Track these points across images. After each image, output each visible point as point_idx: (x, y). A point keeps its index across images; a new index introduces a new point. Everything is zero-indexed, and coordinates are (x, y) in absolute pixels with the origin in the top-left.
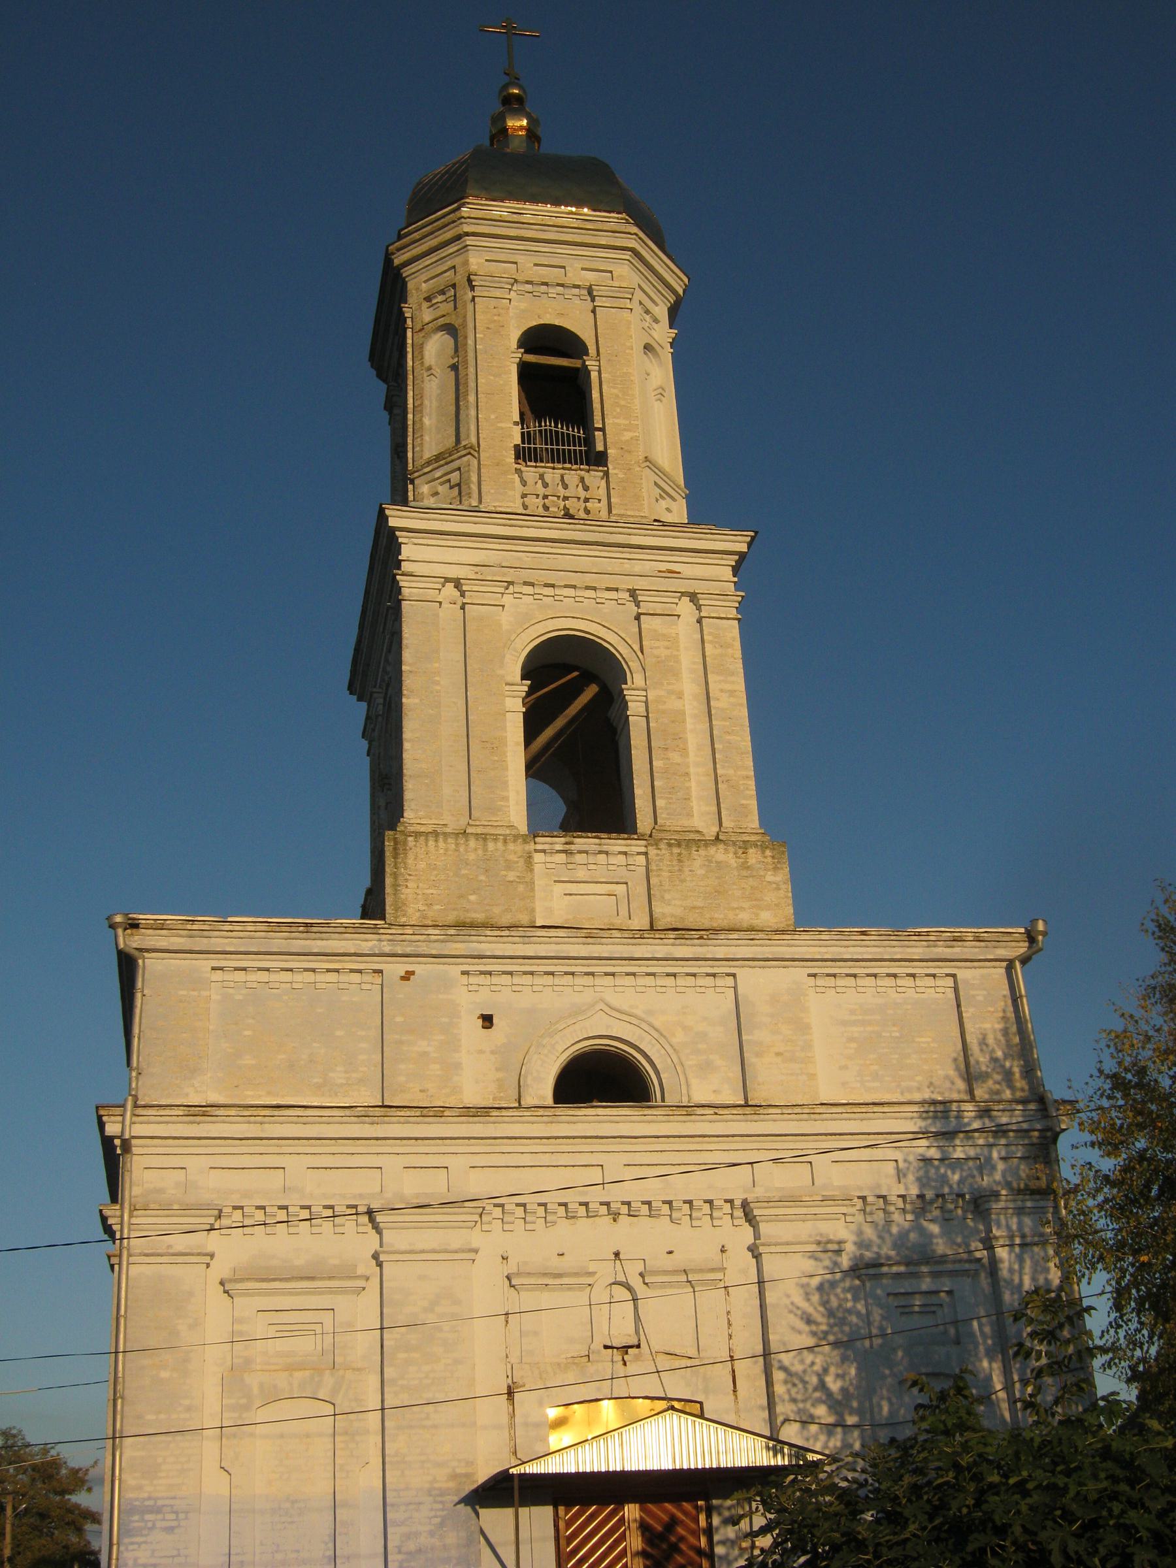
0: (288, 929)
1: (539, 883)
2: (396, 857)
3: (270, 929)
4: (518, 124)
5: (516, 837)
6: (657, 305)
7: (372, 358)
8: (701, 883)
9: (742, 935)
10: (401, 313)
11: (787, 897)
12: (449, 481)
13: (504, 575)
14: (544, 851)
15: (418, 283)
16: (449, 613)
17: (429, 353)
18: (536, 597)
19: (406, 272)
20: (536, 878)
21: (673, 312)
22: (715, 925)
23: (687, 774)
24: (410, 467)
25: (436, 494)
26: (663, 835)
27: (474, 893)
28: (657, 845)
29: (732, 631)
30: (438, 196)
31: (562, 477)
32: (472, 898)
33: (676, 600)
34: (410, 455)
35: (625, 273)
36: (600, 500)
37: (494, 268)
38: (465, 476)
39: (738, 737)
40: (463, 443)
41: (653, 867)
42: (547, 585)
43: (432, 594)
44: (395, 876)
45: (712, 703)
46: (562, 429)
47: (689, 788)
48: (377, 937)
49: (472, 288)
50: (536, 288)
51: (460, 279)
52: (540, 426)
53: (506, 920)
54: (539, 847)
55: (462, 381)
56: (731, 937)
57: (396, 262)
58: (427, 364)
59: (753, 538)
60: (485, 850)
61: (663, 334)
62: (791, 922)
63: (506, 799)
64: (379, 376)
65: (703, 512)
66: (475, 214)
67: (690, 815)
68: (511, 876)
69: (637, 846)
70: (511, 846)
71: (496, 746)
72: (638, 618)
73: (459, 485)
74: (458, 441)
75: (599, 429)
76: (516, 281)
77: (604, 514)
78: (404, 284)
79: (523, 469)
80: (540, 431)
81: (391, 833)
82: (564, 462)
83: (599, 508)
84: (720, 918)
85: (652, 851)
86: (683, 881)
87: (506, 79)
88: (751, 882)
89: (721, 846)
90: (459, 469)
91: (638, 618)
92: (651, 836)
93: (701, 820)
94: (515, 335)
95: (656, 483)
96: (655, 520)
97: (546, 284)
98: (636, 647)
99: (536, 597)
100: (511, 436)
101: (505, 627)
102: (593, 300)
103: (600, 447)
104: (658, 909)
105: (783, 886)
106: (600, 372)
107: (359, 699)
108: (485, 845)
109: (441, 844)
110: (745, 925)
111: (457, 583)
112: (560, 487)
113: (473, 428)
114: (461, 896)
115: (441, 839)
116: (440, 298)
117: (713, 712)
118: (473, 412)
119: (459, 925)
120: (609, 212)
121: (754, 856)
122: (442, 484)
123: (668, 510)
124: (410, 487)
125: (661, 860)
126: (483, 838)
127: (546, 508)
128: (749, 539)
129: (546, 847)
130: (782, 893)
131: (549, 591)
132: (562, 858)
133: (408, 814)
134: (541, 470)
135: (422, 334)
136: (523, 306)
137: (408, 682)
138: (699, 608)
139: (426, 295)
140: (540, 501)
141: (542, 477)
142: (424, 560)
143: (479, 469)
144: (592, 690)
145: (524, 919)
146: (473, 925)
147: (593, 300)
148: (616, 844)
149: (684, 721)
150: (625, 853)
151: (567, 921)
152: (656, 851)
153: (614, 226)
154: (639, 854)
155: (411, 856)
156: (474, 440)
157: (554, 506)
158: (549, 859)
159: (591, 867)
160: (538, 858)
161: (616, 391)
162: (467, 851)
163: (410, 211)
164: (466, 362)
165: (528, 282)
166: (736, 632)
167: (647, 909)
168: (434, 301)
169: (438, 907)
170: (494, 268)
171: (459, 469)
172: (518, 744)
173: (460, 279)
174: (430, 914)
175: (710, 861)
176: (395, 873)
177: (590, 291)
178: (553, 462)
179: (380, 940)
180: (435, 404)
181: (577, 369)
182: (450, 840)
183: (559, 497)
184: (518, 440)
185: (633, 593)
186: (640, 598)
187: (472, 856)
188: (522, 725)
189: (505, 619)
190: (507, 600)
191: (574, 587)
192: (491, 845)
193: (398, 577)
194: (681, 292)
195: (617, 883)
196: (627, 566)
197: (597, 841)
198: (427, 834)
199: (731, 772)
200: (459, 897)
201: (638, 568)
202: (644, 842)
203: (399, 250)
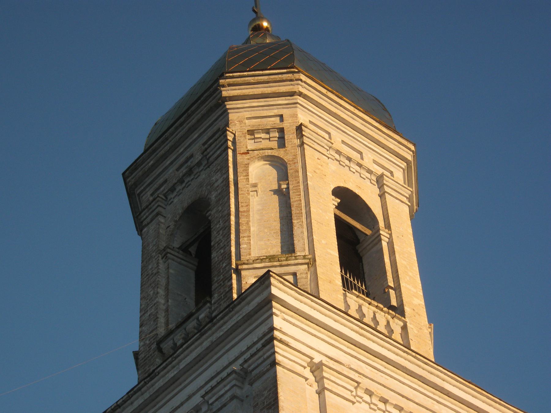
116: (263, 135)
134: (361, 302)
203: (230, 85)
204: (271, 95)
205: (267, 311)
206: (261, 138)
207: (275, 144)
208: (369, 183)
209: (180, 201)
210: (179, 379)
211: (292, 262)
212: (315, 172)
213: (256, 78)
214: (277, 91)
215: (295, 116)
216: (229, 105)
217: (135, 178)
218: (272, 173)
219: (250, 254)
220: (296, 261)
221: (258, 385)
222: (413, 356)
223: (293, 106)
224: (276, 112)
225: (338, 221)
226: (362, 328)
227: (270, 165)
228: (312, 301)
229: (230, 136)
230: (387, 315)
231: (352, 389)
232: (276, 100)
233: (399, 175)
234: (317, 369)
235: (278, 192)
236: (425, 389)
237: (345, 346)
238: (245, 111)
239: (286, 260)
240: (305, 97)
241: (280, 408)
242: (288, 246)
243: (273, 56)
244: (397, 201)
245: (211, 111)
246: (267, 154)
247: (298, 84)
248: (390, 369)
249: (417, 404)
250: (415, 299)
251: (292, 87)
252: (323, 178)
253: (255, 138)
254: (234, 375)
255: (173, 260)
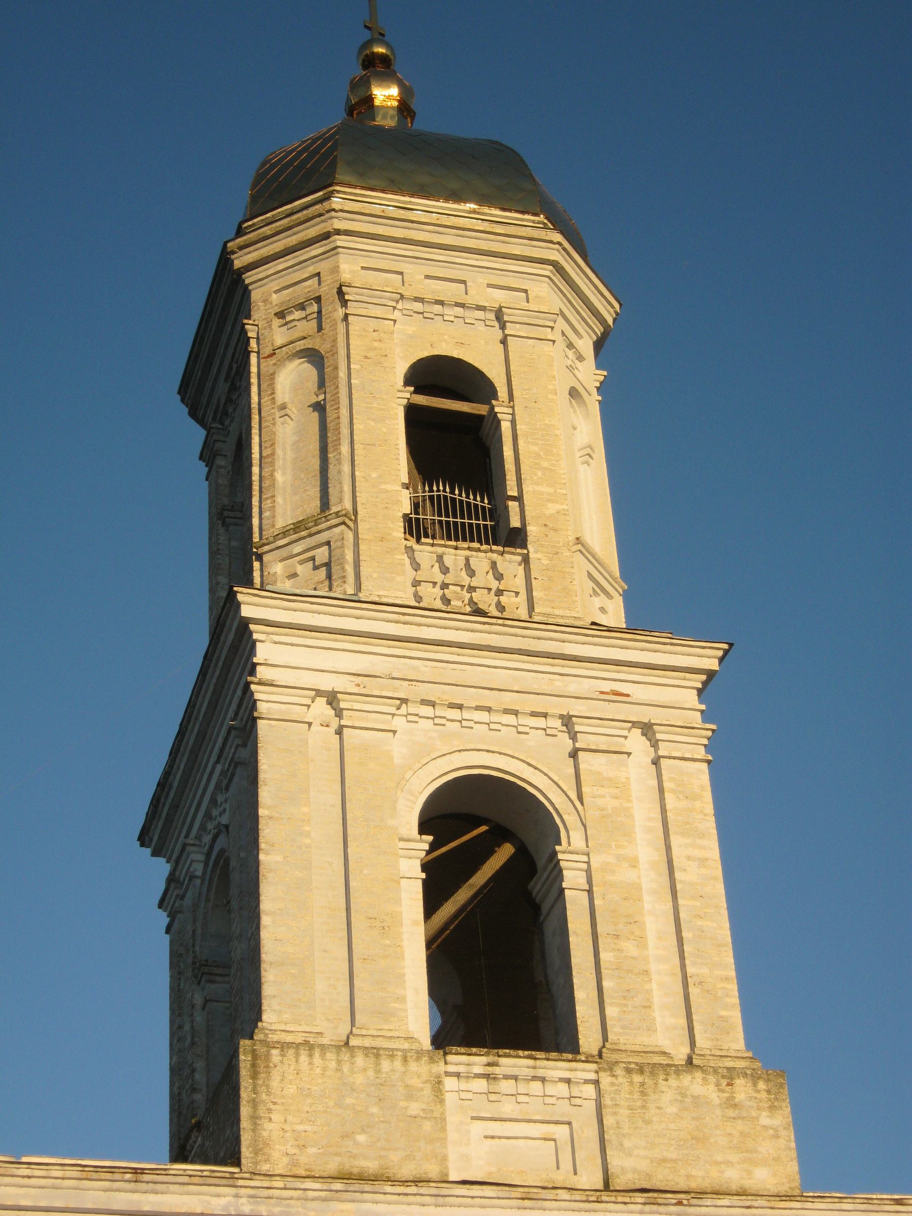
0: (109, 1176)
1: (452, 1119)
2: (255, 1076)
3: (84, 1175)
4: (385, 95)
5: (420, 1054)
6: (580, 336)
7: (183, 390)
8: (672, 1126)
9: (735, 1200)
10: (244, 332)
11: (790, 1149)
12: (313, 559)
13: (395, 689)
14: (458, 1075)
15: (267, 292)
16: (321, 739)
17: (281, 389)
18: (437, 721)
19: (249, 277)
20: (448, 1113)
21: (599, 345)
22: (693, 1185)
23: (646, 972)
24: (256, 539)
25: (295, 575)
26: (615, 1057)
27: (363, 1131)
28: (611, 1070)
29: (701, 776)
30: (294, 180)
31: (467, 559)
32: (361, 1138)
33: (625, 733)
34: (255, 521)
35: (545, 294)
36: (517, 593)
37: (372, 278)
38: (336, 553)
39: (712, 924)
40: (334, 509)
41: (607, 1101)
42: (452, 706)
43: (297, 712)
44: (254, 1104)
45: (678, 875)
46: (459, 495)
47: (649, 992)
48: (233, 1191)
49: (345, 303)
50: (428, 308)
51: (327, 290)
52: (431, 490)
53: (407, 1171)
54: (451, 1068)
55: (331, 425)
56: (720, 1202)
57: (238, 264)
58: (279, 401)
59: (726, 652)
60: (378, 1071)
61: (590, 375)
62: (797, 1183)
63: (402, 999)
64: (193, 414)
65: (649, 613)
66: (349, 206)
67: (651, 1029)
68: (415, 1108)
69: (586, 1071)
70: (413, 1066)
71: (387, 926)
72: (574, 754)
73: (328, 565)
74: (325, 504)
75: (514, 498)
76: (402, 297)
77: (523, 613)
78: (246, 292)
79: (416, 547)
80: (431, 498)
81: (248, 1042)
82: (472, 540)
83: (516, 604)
84: (699, 1175)
85: (605, 1080)
86: (648, 1122)
87: (367, 35)
88: (740, 1126)
89: (698, 1075)
90: (328, 543)
91: (574, 754)
92: (600, 1055)
93: (668, 1037)
94: (402, 368)
95: (589, 573)
96: (593, 623)
97: (442, 303)
98: (573, 795)
99: (437, 721)
100: (398, 502)
101: (397, 760)
102: (503, 327)
103: (515, 523)
104: (616, 1161)
105: (783, 1133)
106: (513, 422)
107: (155, 854)
108: (377, 1064)
109: (317, 1060)
110: (734, 1187)
111: (332, 698)
112: (464, 573)
113: (347, 488)
114: (345, 1136)
115: (317, 1053)
116: (298, 314)
117: (679, 887)
118: (346, 468)
119: (345, 1177)
120: (523, 213)
121: (742, 1089)
122: (301, 562)
123: (603, 610)
124: (256, 565)
125: (618, 1092)
126: (375, 1053)
127: (446, 601)
128: (720, 653)
129: (461, 1069)
130: (782, 1142)
131: (455, 714)
132: (481, 1085)
133: (268, 1016)
134: (440, 550)
135: (272, 361)
136: (410, 330)
137: (268, 832)
138: (655, 744)
139: (277, 310)
140: (437, 592)
141: (440, 559)
142: (288, 664)
143: (356, 545)
144: (506, 851)
145: (432, 1170)
146: (362, 1178)
147: (503, 327)
148: (555, 1068)
149: (640, 899)
150: (568, 1081)
151: (490, 1173)
152: (609, 1079)
153: (529, 235)
154: (586, 1082)
155: (276, 1075)
156: (348, 505)
157: (459, 599)
158: (464, 1085)
159: (521, 1098)
160: (450, 1083)
161: (535, 448)
162: (352, 1072)
163: (254, 199)
164: (337, 401)
165: (417, 299)
166: (705, 778)
167: (599, 1161)
168: (289, 318)
169: (315, 1150)
170: (372, 278)
171: (328, 543)
172: (415, 923)
173: (327, 290)
174: (303, 1159)
175: (684, 1096)
176: (254, 1100)
177: (499, 315)
178: (457, 540)
179: (237, 1196)
180: (290, 454)
181: (480, 418)
182: (329, 1055)
183: (462, 587)
184: (407, 508)
185: (567, 720)
186: (577, 728)
187: (359, 1079)
188: (421, 896)
189: (397, 748)
190: (398, 723)
191: (489, 709)
192: (385, 1065)
193: (253, 687)
194: (610, 321)
195: (557, 1123)
196: (558, 684)
197: (530, 1062)
198: (297, 1046)
199: (705, 971)
200: (343, 1137)
201: (573, 686)
202: (594, 1066)
203: (241, 248)
204: (299, 247)
205: (248, 641)
206: (294, 320)
208: (484, 328)
210: (206, 733)
211: (323, 526)
212: (366, 357)
213: (274, 225)
214: (305, 239)
215: (335, 270)
219: (273, 526)
220: (328, 524)
222: (500, 625)
223: (332, 253)
226: (404, 614)
227: (308, 362)
228: (312, 603)
229: (252, 331)
230: (489, 554)
231: (393, 710)
232: (308, 252)
236: (534, 663)
238: (271, 281)
239: (316, 525)
240: (347, 233)
241: (260, 783)
244: (530, 342)
246: (298, 349)
247: (332, 218)
249: (518, 692)
250: (550, 505)
251: (323, 225)
253: (286, 324)
254: (233, 733)
255: (236, 524)
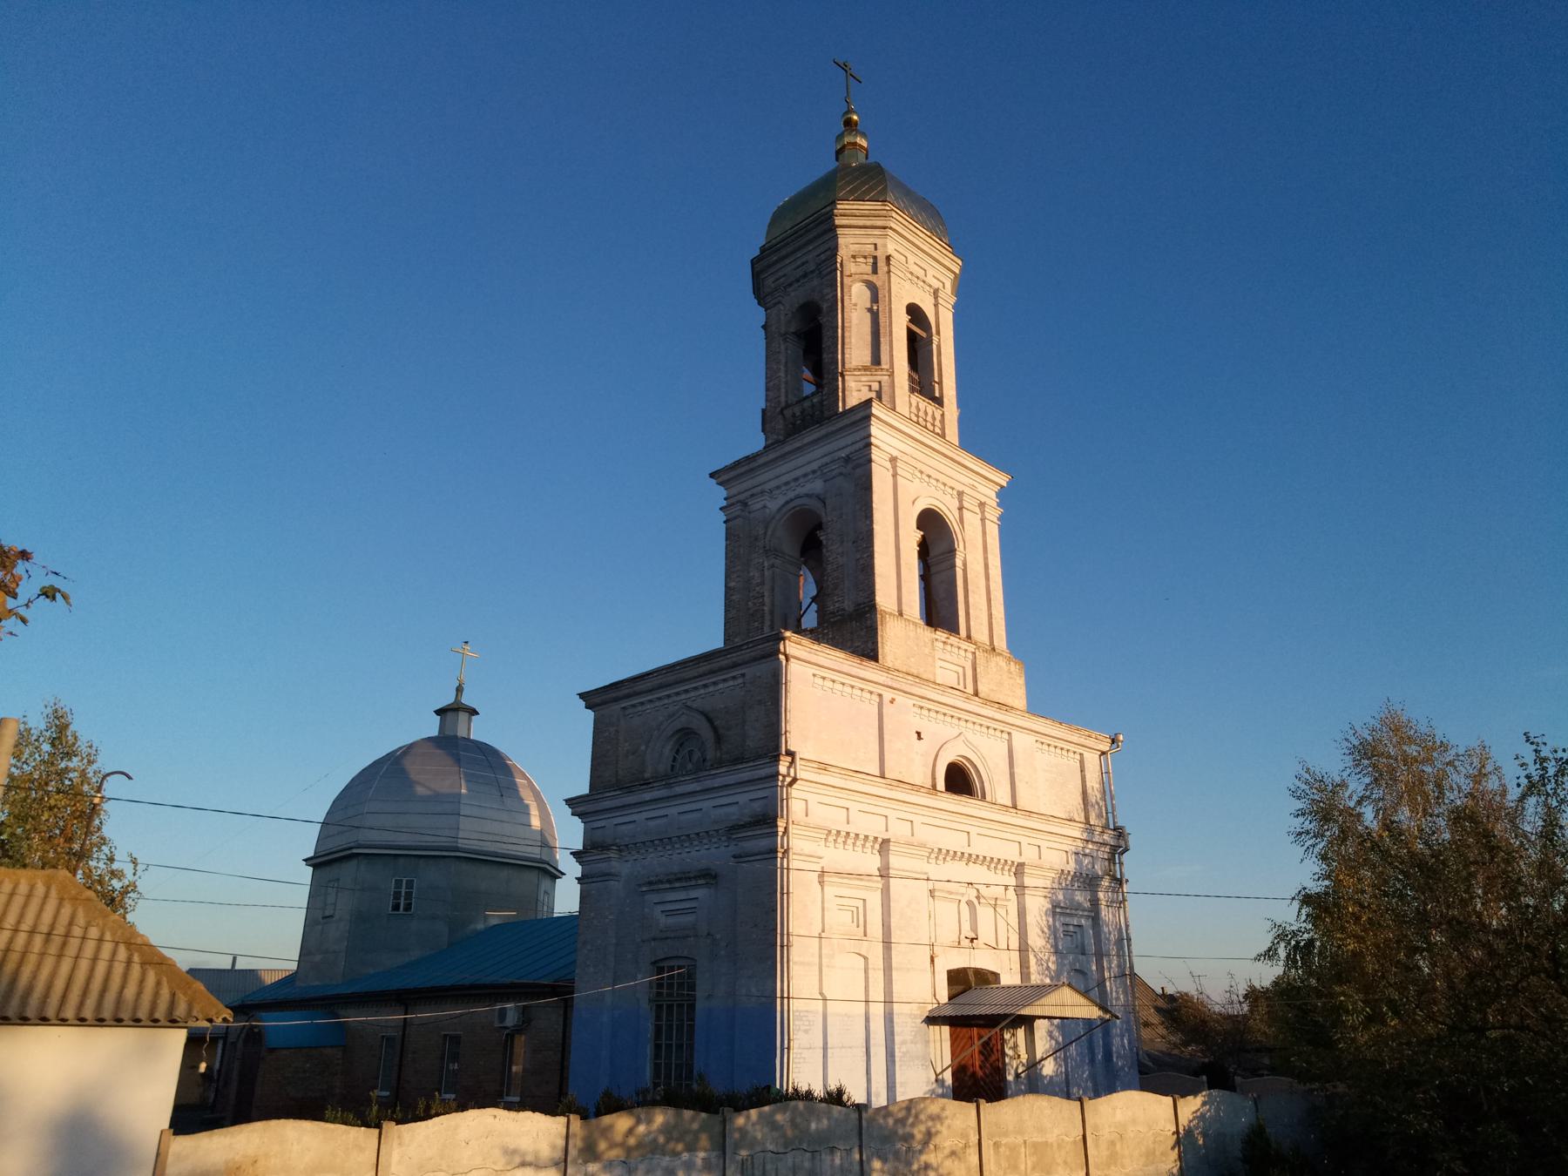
207: (869, 269)
209: (795, 297)
216: (839, 231)
217: (760, 268)
218: (867, 293)
221: (859, 471)
224: (872, 240)
225: (909, 331)
233: (948, 285)
234: (893, 460)
235: (870, 310)
237: (909, 441)
242: (876, 360)
243: (870, 180)
245: (825, 232)
248: (996, 826)
252: (903, 293)
